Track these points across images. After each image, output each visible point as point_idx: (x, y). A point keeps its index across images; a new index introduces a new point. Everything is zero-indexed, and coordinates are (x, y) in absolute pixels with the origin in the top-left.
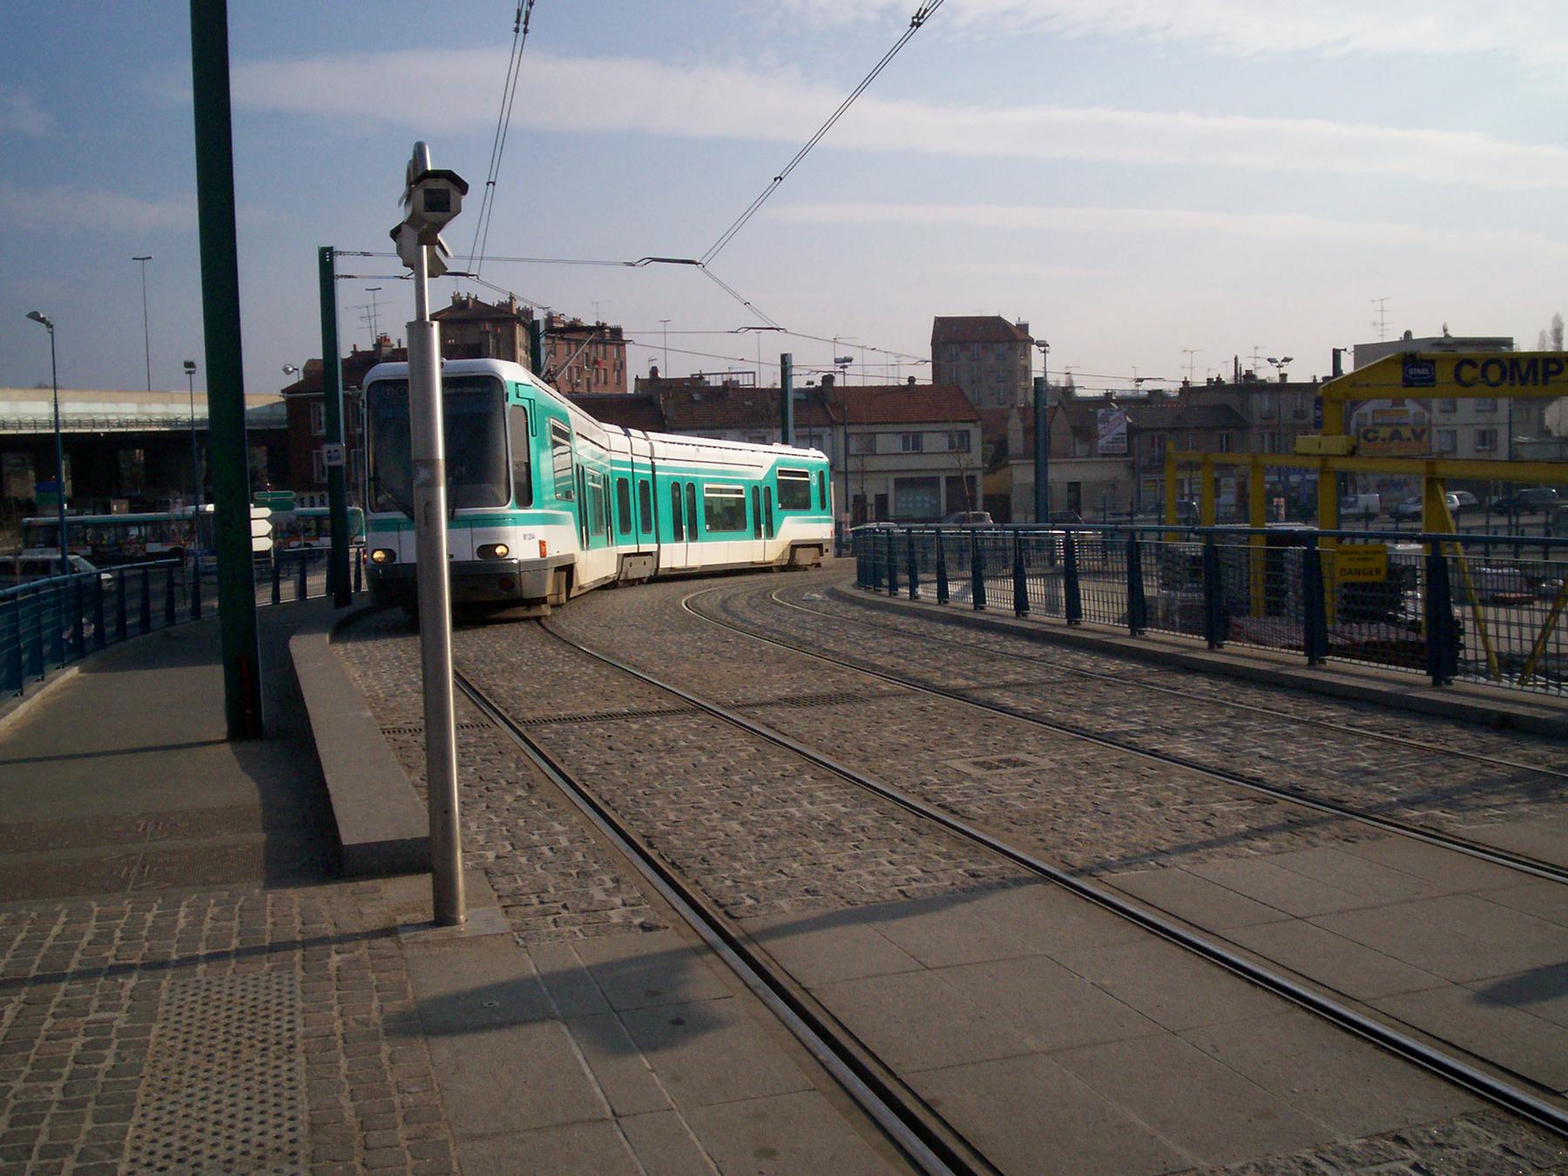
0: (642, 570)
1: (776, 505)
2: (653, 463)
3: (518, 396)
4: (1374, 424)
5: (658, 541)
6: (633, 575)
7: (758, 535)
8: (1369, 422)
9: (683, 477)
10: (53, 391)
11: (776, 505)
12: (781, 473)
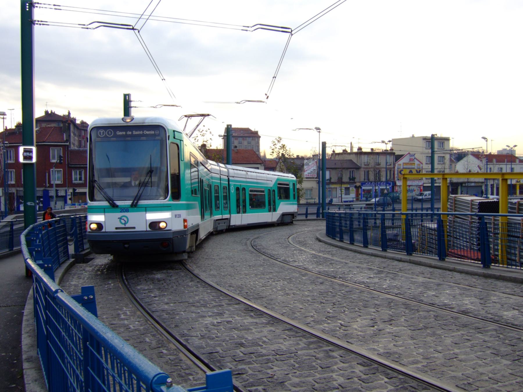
0: (222, 226)
1: (277, 198)
2: (229, 179)
3: (174, 138)
4: (403, 168)
5: (230, 213)
6: (219, 228)
7: (270, 211)
8: (402, 167)
9: (241, 185)
10: (411, 204)
11: (277, 198)
12: (279, 184)
